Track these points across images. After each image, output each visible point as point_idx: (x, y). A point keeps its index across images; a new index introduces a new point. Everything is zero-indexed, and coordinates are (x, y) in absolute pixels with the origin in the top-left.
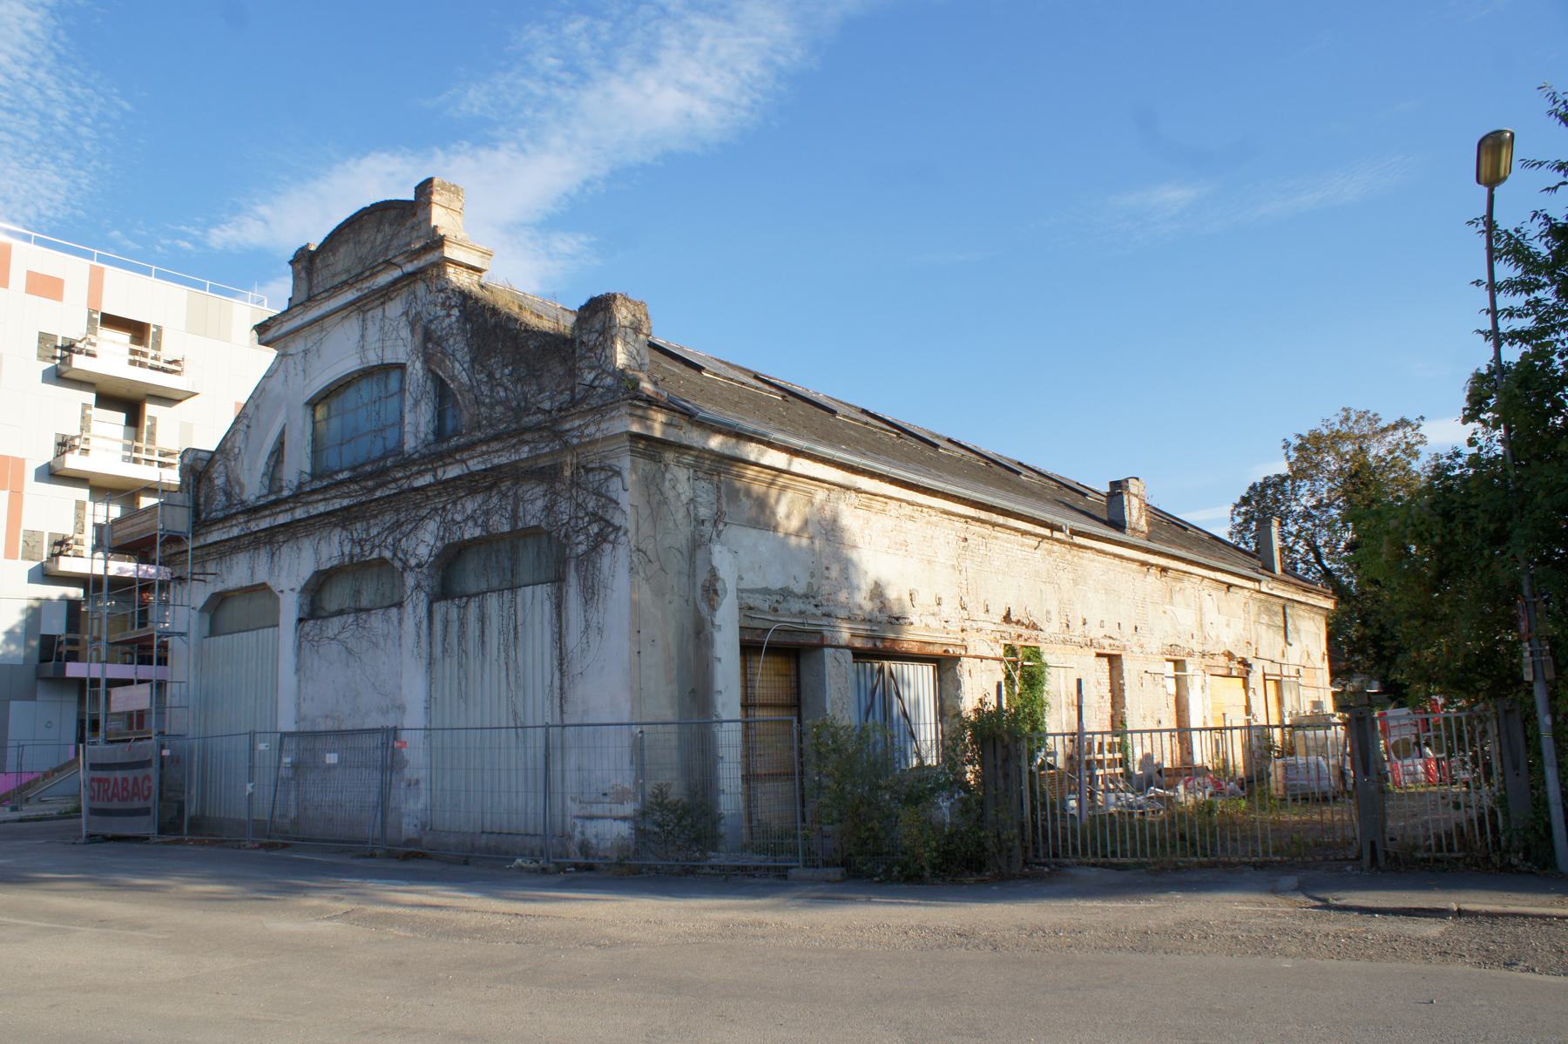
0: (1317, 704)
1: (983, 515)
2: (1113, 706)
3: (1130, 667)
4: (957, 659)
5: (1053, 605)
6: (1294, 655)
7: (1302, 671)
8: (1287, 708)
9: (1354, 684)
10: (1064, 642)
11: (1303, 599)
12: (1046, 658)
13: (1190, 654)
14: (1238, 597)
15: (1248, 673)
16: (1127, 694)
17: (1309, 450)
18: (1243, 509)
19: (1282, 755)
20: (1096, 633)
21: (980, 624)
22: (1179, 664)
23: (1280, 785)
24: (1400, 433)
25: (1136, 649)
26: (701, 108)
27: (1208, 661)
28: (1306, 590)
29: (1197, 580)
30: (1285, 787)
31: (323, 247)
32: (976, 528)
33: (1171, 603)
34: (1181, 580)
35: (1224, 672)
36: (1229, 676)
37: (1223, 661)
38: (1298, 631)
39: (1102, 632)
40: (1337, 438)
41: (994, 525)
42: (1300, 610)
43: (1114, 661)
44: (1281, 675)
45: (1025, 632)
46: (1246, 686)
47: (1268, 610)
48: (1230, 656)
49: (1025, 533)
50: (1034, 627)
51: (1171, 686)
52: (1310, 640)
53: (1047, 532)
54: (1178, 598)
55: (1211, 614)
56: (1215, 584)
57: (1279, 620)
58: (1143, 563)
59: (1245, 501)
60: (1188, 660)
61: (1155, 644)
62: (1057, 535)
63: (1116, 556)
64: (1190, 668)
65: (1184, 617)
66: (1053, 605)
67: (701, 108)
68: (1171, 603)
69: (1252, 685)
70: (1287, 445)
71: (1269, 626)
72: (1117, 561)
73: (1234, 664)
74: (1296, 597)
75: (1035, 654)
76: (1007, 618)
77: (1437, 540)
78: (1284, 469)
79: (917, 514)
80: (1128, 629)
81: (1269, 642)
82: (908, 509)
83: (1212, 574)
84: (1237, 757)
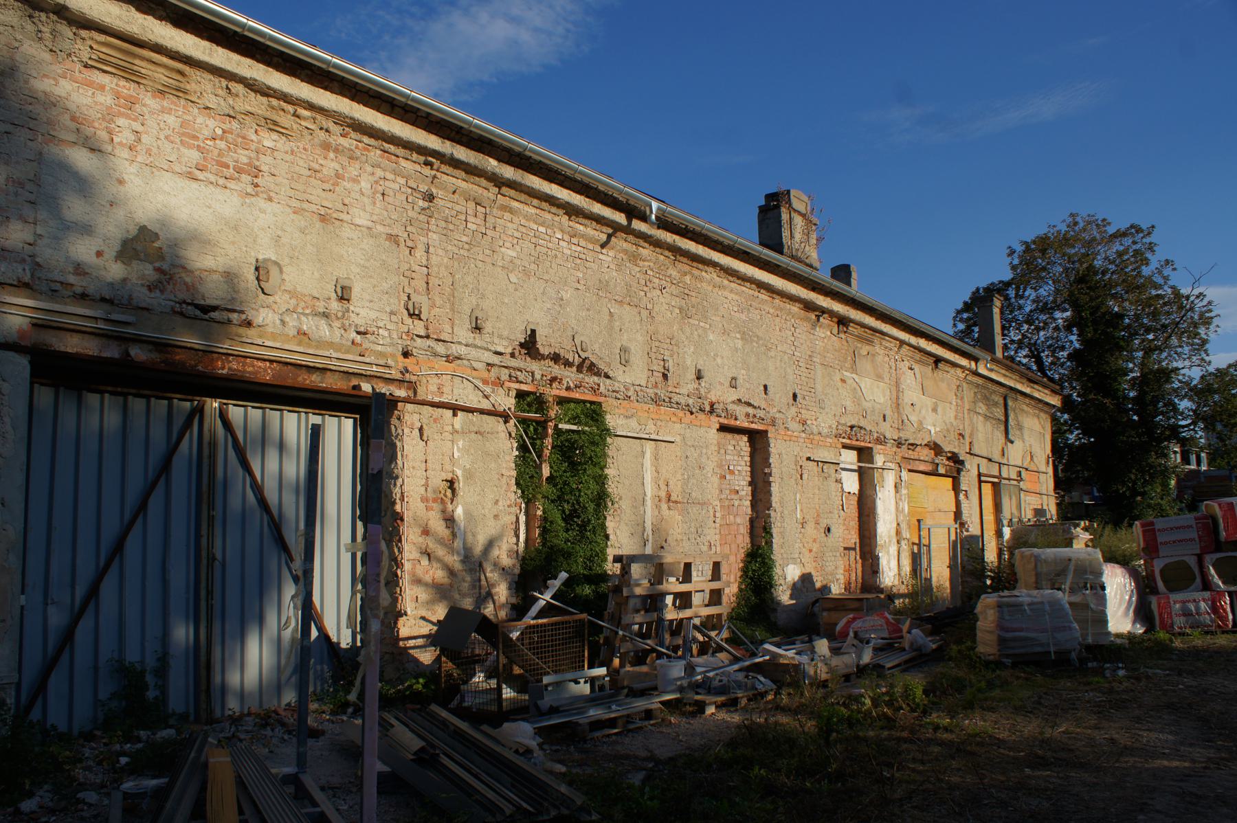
0: (1039, 512)
1: (462, 153)
2: (754, 504)
3: (781, 452)
4: (390, 404)
5: (636, 343)
6: (1016, 454)
7: (1024, 473)
9: (1075, 496)
10: (656, 401)
11: (1028, 390)
12: (611, 421)
13: (881, 441)
14: (949, 377)
15: (959, 471)
16: (775, 488)
17: (1032, 259)
18: (965, 316)
19: (995, 588)
20: (721, 394)
21: (456, 350)
22: (864, 454)
23: (992, 638)
24: (1128, 241)
25: (794, 426)
26: (525, 36)
27: (904, 451)
28: (1031, 381)
29: (893, 345)
30: (1002, 641)
32: (453, 180)
33: (854, 369)
35: (929, 468)
36: (934, 473)
37: (926, 454)
38: (1020, 427)
39: (733, 395)
40: (1065, 241)
41: (499, 182)
42: (1023, 404)
43: (758, 440)
44: (1000, 477)
45: (570, 376)
46: (956, 488)
47: (986, 399)
48: (936, 448)
49: (572, 211)
50: (593, 369)
51: (851, 483)
52: (1032, 443)
53: (620, 218)
55: (911, 393)
56: (918, 356)
58: (809, 306)
59: (967, 307)
60: (877, 448)
61: (825, 422)
62: (637, 225)
63: (761, 285)
64: (879, 460)
65: (876, 394)
66: (636, 343)
67: (525, 36)
69: (963, 487)
70: (1012, 252)
71: (986, 417)
72: (764, 296)
73: (941, 460)
74: (1019, 387)
75: (594, 413)
76: (529, 345)
78: (1008, 275)
79: (286, 120)
80: (780, 396)
81: (986, 437)
82: (257, 103)
83: (913, 340)
84: (940, 572)
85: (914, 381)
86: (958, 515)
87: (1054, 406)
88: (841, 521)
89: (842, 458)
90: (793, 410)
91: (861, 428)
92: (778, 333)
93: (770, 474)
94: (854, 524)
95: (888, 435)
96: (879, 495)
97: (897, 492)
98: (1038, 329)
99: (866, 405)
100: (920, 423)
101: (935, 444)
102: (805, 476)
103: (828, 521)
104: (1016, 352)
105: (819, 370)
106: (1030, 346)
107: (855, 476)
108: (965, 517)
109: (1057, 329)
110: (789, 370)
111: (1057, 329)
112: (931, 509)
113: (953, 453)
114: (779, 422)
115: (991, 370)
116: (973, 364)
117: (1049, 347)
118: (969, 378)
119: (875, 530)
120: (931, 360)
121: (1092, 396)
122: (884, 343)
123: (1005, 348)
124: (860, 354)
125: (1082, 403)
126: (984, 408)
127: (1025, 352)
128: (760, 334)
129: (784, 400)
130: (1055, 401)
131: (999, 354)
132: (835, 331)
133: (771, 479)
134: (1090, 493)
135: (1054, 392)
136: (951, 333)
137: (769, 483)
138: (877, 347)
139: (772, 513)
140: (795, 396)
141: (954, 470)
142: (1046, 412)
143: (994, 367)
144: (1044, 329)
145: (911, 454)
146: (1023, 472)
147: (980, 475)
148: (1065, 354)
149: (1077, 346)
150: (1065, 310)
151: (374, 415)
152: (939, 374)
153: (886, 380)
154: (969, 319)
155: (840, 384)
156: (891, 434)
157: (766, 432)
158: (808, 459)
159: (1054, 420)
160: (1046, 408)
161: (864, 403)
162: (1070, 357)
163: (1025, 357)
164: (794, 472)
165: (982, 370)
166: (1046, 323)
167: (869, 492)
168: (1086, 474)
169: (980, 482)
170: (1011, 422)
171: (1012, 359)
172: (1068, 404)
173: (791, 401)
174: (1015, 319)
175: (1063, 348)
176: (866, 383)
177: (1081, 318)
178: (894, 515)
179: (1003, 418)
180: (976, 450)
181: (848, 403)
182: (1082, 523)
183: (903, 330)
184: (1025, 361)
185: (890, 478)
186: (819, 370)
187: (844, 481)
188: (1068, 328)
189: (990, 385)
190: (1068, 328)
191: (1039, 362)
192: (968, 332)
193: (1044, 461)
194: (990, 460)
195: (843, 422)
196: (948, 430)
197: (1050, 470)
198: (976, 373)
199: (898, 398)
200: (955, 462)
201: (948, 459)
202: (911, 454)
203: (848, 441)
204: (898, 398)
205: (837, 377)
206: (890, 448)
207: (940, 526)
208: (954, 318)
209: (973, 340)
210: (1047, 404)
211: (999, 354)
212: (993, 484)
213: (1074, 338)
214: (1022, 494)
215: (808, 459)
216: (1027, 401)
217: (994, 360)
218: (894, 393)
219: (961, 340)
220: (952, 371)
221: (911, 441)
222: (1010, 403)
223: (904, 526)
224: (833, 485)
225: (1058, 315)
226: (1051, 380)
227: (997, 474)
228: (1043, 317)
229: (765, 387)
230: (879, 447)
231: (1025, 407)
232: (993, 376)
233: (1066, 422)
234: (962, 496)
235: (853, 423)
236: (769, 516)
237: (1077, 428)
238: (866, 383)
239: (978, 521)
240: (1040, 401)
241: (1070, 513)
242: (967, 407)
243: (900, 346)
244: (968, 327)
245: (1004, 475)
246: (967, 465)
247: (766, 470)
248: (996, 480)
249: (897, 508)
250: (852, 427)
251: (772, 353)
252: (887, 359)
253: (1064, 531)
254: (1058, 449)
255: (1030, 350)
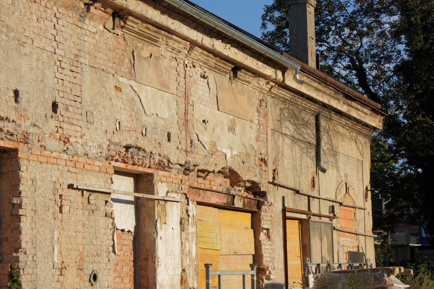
0: (355, 256)
6: (328, 185)
7: (338, 209)
8: (316, 257)
9: (400, 236)
11: (344, 108)
14: (250, 91)
15: (259, 205)
16: (25, 225)
22: (143, 181)
25: (54, 144)
27: (192, 179)
28: (348, 97)
29: (182, 45)
31: (255, 252)
33: (132, 73)
34: (153, 41)
35: (222, 200)
36: (229, 207)
37: (220, 183)
38: (334, 153)
44: (309, 213)
46: (256, 226)
47: (294, 117)
48: (233, 176)
51: (126, 218)
52: (348, 171)
54: (146, 70)
55: (203, 107)
56: (213, 61)
57: (309, 134)
60: (159, 175)
61: (94, 139)
64: (161, 190)
65: (160, 107)
68: (132, 73)
69: (265, 224)
71: (294, 139)
73: (239, 191)
74: (334, 104)
77: (382, 261)
80: (35, 106)
81: (293, 164)
83: (207, 41)
85: (206, 90)
86: (257, 257)
87: (375, 129)
88: (111, 266)
89: (114, 187)
90: (53, 124)
91: (139, 149)
92: (35, 24)
93: (20, 206)
94: (128, 269)
95: (173, 159)
96: (160, 233)
97: (182, 230)
98: (361, 35)
99: (147, 120)
100: (214, 144)
101: (232, 171)
102: (66, 209)
103: (95, 267)
104: (335, 61)
105: (88, 75)
106: (350, 54)
107: (131, 209)
108: (266, 261)
109: (382, 35)
110: (48, 72)
111: (382, 35)
112: (225, 251)
113: (253, 183)
114: (33, 138)
115: (301, 82)
116: (280, 73)
117: (373, 56)
118: (275, 91)
119: (155, 278)
120: (229, 67)
121: (420, 118)
122: (171, 43)
123: (320, 56)
124: (140, 57)
125: (410, 126)
126: (291, 128)
127: (346, 62)
128: (11, 24)
129: (41, 111)
130: (376, 122)
131: (312, 63)
132: (110, 25)
133: (21, 212)
134: (418, 234)
135: (374, 111)
136: (259, 36)
137: (18, 217)
138: (163, 48)
139: (21, 256)
140: (55, 106)
141: (254, 203)
142: (365, 136)
143: (305, 79)
144: (367, 34)
145: (201, 183)
146: (337, 206)
147: (284, 210)
148: (392, 66)
149: (406, 57)
150: (392, 14)
151: (204, 179)
152: (238, 85)
153: (173, 89)
154: (282, 19)
155: (113, 92)
156: (177, 157)
157: (16, 151)
158: (71, 186)
159: (375, 146)
160: (365, 131)
161: (144, 118)
162: (397, 70)
163: (346, 68)
164: (52, 203)
165: (290, 82)
166: (369, 27)
167: (148, 230)
168: (412, 210)
169: (285, 218)
170: (324, 146)
171: (330, 70)
172: (391, 126)
173: (50, 112)
174: (335, 21)
175: (388, 59)
176: (147, 93)
177: (411, 24)
178: (178, 259)
179: (314, 141)
180: (280, 180)
181: (124, 118)
182: (397, 270)
183: (195, 28)
184: (344, 73)
185: (174, 212)
186: (88, 75)
187: (115, 215)
188: (396, 36)
189: (299, 100)
190: (396, 36)
191: (361, 74)
192: (278, 35)
193: (361, 195)
194: (297, 192)
195: (116, 139)
196: (247, 155)
197: (369, 205)
198: (283, 86)
199: (186, 113)
200: (255, 194)
201: (247, 189)
202: (201, 183)
203: (123, 165)
204: (186, 113)
205: (111, 84)
206: (175, 175)
207: (233, 272)
208: (264, 17)
209: (285, 45)
210: (366, 125)
211: (312, 63)
212: (301, 221)
213: (401, 47)
214: (335, 233)
215: (71, 186)
216: (343, 121)
217: (303, 70)
218: (182, 107)
219: (271, 46)
220: (254, 81)
221: (202, 167)
222: (323, 123)
223: (190, 272)
224: (102, 221)
225: (384, 18)
226: (374, 97)
227: (306, 209)
228: (367, 20)
229: (16, 93)
230: (161, 173)
231: (340, 129)
232: (303, 89)
233: (390, 147)
234: (262, 236)
235: (130, 142)
236: (17, 260)
237: (403, 157)
238: (147, 93)
239: (282, 266)
240: (358, 122)
241: (388, 256)
242: (271, 126)
243: (191, 49)
244: (279, 29)
245: (314, 210)
246: (270, 198)
247: (15, 201)
248: (304, 217)
249: (182, 251)
250: (127, 148)
251: (27, 50)
252: (174, 63)
253: (376, 278)
254: (379, 181)
255: (352, 60)
